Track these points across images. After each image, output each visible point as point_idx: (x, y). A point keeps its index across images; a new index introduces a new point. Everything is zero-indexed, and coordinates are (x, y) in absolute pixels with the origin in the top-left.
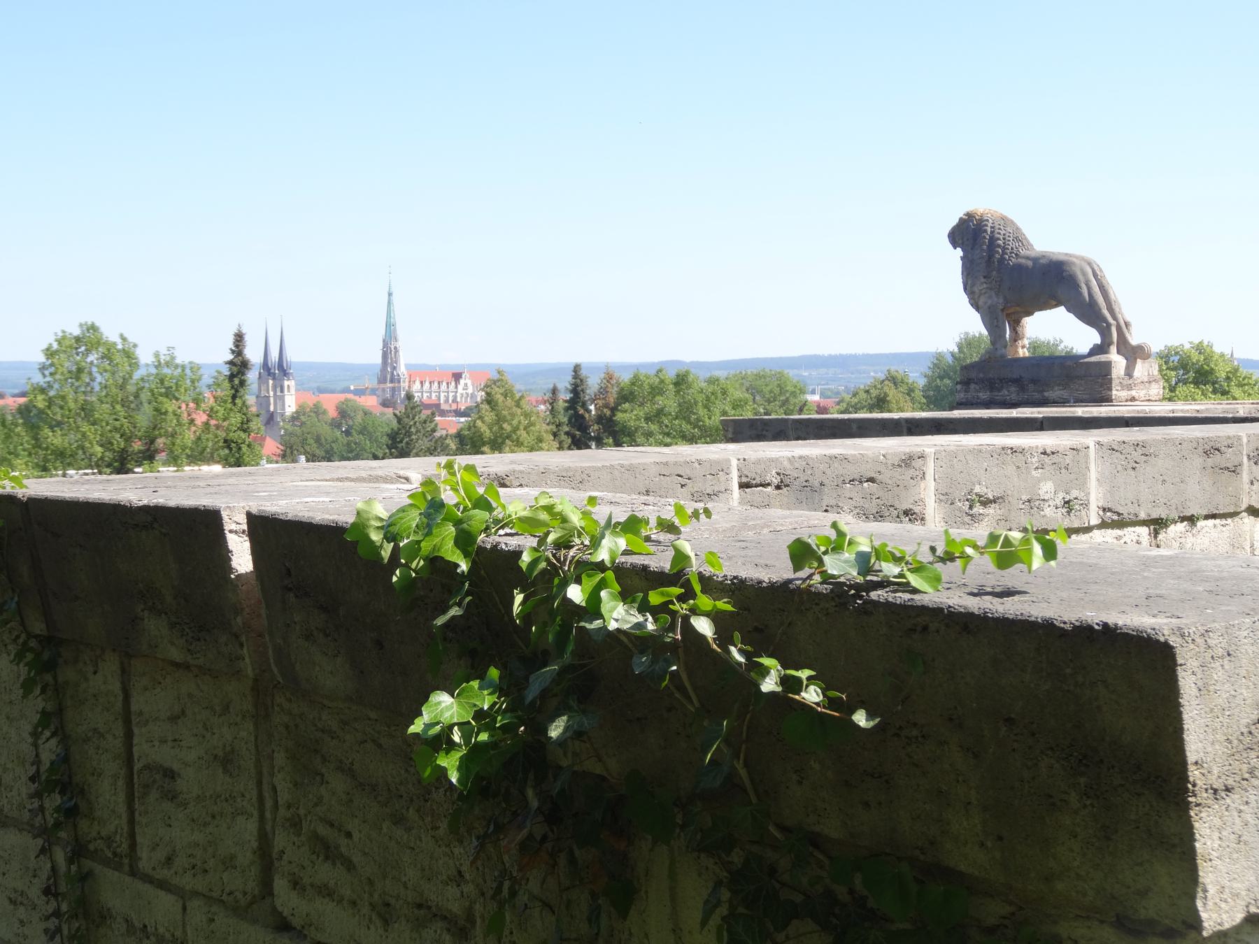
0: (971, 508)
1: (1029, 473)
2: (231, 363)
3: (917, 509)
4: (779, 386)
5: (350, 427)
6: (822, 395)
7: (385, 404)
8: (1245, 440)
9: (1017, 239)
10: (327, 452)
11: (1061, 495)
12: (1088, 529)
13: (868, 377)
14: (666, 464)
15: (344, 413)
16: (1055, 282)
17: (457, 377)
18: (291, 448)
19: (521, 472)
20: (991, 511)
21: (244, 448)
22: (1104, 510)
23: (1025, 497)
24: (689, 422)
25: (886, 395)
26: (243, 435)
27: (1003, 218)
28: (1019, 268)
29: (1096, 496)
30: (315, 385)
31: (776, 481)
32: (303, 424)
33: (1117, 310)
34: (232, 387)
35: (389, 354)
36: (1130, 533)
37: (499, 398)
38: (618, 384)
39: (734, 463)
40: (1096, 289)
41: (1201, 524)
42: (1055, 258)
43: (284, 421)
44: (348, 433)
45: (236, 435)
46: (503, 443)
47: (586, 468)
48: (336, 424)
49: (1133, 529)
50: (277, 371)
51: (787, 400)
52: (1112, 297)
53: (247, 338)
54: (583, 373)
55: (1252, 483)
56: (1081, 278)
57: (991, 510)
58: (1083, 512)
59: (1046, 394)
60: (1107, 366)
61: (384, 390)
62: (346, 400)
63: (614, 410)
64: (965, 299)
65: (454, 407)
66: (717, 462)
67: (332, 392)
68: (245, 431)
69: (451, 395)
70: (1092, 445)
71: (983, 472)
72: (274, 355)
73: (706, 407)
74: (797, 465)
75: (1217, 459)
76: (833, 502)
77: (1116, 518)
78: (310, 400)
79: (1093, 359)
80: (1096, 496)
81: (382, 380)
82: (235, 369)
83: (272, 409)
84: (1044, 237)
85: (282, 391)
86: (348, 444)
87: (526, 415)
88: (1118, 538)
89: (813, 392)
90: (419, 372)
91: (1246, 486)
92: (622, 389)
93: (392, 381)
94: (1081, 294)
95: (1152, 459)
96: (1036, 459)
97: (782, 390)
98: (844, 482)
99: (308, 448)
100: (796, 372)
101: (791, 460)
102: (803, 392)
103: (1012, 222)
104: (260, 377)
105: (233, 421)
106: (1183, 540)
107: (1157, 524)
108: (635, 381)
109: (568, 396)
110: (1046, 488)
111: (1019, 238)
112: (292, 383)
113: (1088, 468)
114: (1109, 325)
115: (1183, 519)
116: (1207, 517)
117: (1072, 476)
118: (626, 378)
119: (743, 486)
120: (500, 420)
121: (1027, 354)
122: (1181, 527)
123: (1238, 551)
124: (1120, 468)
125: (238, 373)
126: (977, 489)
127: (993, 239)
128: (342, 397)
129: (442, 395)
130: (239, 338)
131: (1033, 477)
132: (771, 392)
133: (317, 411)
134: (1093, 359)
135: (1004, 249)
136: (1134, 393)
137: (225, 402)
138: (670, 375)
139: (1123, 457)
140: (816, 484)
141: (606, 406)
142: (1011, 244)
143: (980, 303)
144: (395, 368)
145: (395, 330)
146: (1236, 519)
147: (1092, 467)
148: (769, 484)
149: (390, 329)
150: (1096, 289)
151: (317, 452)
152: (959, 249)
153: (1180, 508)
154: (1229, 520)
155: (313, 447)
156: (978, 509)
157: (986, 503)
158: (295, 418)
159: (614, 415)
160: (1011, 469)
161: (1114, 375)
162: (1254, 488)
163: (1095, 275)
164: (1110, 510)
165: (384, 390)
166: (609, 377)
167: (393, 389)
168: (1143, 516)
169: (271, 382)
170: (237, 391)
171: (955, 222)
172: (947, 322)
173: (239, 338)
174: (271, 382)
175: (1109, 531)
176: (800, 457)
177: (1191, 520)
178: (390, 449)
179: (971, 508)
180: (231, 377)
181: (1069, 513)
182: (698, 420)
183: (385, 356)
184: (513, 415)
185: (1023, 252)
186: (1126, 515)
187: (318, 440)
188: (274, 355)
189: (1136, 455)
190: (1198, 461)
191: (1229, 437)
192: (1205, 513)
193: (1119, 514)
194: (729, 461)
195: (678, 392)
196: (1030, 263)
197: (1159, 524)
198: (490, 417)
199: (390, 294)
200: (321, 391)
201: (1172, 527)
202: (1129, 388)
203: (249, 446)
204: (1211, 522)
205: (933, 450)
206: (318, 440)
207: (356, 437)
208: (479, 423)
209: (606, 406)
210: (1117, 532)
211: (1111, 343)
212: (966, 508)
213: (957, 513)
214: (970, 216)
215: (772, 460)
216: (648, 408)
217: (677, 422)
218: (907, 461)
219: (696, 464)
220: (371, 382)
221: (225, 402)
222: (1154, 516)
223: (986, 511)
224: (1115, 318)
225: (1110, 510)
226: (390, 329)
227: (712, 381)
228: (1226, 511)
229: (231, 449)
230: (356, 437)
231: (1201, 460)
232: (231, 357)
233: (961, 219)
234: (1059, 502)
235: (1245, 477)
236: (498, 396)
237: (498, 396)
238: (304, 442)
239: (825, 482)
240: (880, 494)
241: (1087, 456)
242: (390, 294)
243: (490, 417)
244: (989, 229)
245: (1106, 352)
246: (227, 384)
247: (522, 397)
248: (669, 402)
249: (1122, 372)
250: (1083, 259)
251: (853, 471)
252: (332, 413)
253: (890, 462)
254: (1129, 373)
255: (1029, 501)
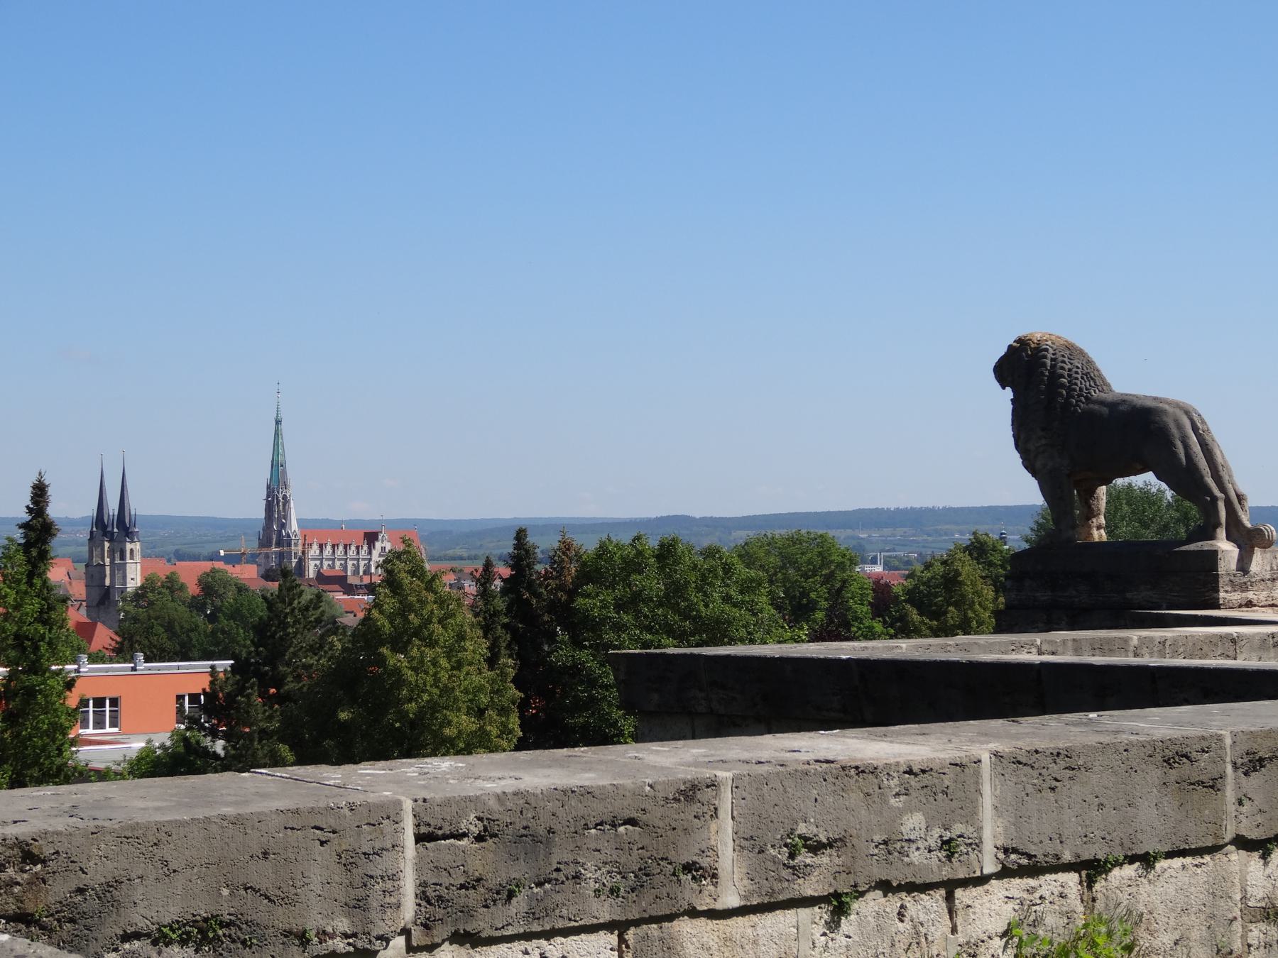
0: (792, 856)
1: (886, 802)
2: (25, 526)
3: (704, 862)
4: (820, 554)
5: (217, 610)
6: (887, 565)
7: (268, 576)
8: (1228, 741)
9: (1087, 375)
10: (183, 645)
11: (936, 832)
12: (982, 880)
13: (940, 545)
14: (297, 811)
15: (209, 586)
16: (1144, 434)
17: (371, 538)
18: (131, 639)
19: (58, 833)
20: (825, 860)
21: (43, 647)
22: (1006, 851)
23: (878, 838)
24: (676, 609)
25: (958, 573)
26: (41, 629)
27: (1070, 347)
28: (1090, 415)
29: (992, 831)
30: (171, 548)
31: (475, 831)
32: (151, 603)
33: (1226, 478)
34: (29, 561)
35: (275, 504)
36: (1048, 884)
37: (406, 579)
38: (578, 556)
39: (408, 805)
40: (1197, 448)
41: (1161, 865)
42: (1139, 403)
43: (124, 600)
44: (212, 618)
45: (32, 628)
46: (409, 641)
47: (163, 824)
48: (196, 605)
49: (1054, 876)
50: (112, 529)
51: (832, 574)
52: (1219, 459)
53: (50, 491)
54: (531, 539)
55: (1240, 803)
56: (1174, 431)
57: (824, 859)
58: (973, 856)
59: (1129, 595)
60: (1213, 556)
61: (267, 556)
62: (213, 570)
63: (572, 594)
64: (1016, 458)
65: (366, 580)
66: (381, 806)
67: (196, 558)
68: (44, 623)
69: (362, 563)
70: (985, 757)
71: (810, 803)
72: (112, 506)
73: (699, 589)
74: (509, 805)
75: (1185, 769)
76: (568, 857)
77: (1024, 861)
78: (162, 569)
79: (1193, 547)
80: (992, 831)
81: (265, 542)
82: (33, 535)
83: (107, 583)
84: (1127, 374)
85: (123, 557)
86: (213, 633)
87: (441, 602)
88: (1030, 891)
89: (874, 561)
90: (317, 530)
91: (1231, 807)
92: (584, 564)
93: (279, 544)
94: (1175, 455)
95: (1082, 775)
96: (896, 781)
97: (825, 562)
98: (586, 827)
99: (154, 639)
100: (849, 532)
101: (501, 797)
102: (853, 562)
103: (1081, 352)
104: (91, 539)
105: (28, 608)
106: (1133, 890)
107: (1092, 869)
108: (603, 551)
109: (506, 572)
110: (913, 823)
111: (1091, 374)
112: (137, 546)
113: (979, 792)
114: (1214, 499)
115: (1131, 859)
116: (1170, 855)
117: (955, 804)
118: (589, 545)
119: (420, 838)
120: (405, 608)
121: (1105, 538)
122: (1130, 871)
123: (1222, 903)
124: (1030, 789)
125: (37, 541)
126: (802, 829)
127: (1054, 376)
128: (207, 566)
129: (350, 563)
130: (40, 492)
131: (891, 808)
132: (809, 562)
133: (172, 584)
134: (1193, 547)
135: (1070, 390)
136: (1250, 595)
137: (18, 582)
138: (653, 543)
139: (1035, 773)
140: (541, 831)
141: (561, 587)
142: (1080, 384)
143: (1038, 465)
144: (283, 526)
145: (284, 472)
146: (1218, 856)
147: (987, 789)
148: (464, 835)
149: (277, 466)
150: (1197, 448)
151: (168, 645)
152: (1008, 389)
153: (1127, 843)
154: (1207, 858)
155: (162, 637)
156: (805, 858)
157: (816, 848)
158: (140, 594)
159: (573, 601)
160: (855, 798)
161: (1221, 571)
162: (1244, 809)
163: (1195, 428)
164: (1015, 851)
165: (267, 556)
166: (566, 547)
167: (281, 555)
168: (1067, 857)
169: (107, 545)
170: (35, 566)
171: (1002, 351)
172: (997, 484)
173: (40, 492)
174: (107, 545)
175: (1017, 881)
176: (516, 794)
177: (1147, 860)
178: (257, 647)
179: (792, 856)
180: (27, 547)
181: (949, 858)
182: (691, 606)
183: (269, 508)
184: (423, 602)
185: (1095, 394)
186: (1040, 858)
187: (169, 627)
188: (112, 506)
189: (1057, 769)
190: (1156, 773)
191: (1203, 738)
192: (1167, 848)
193: (1030, 856)
194: (398, 804)
195: (662, 568)
196: (1105, 410)
197: (1095, 868)
198: (390, 604)
199: (278, 422)
200: (180, 556)
201: (1116, 872)
202: (1244, 588)
203: (50, 644)
204: (1177, 862)
205: (729, 775)
206: (169, 627)
207: (224, 622)
208: (375, 613)
209: (561, 587)
210: (1031, 882)
211: (1219, 525)
212: (784, 857)
213: (770, 865)
214: (1022, 342)
215: (469, 799)
216: (619, 590)
217: (660, 612)
218: (690, 792)
219: (346, 811)
220: (249, 545)
221: (18, 582)
222: (1086, 856)
223: (817, 860)
224: (1223, 489)
225: (1015, 851)
226: (277, 466)
227: (710, 553)
228: (1200, 844)
229: (24, 649)
230: (224, 622)
231: (1159, 772)
232: (26, 517)
233: (1010, 347)
234: (933, 841)
235: (1230, 794)
236: (403, 575)
237: (403, 575)
238: (149, 631)
239: (556, 827)
240: (646, 842)
241: (977, 774)
242: (278, 422)
243: (390, 604)
244: (1048, 362)
245: (1212, 537)
246: (20, 557)
247: (433, 579)
248: (653, 584)
249: (1233, 566)
250: (1178, 405)
251: (598, 810)
252: (193, 589)
253: (660, 795)
254: (1243, 566)
255: (885, 843)
